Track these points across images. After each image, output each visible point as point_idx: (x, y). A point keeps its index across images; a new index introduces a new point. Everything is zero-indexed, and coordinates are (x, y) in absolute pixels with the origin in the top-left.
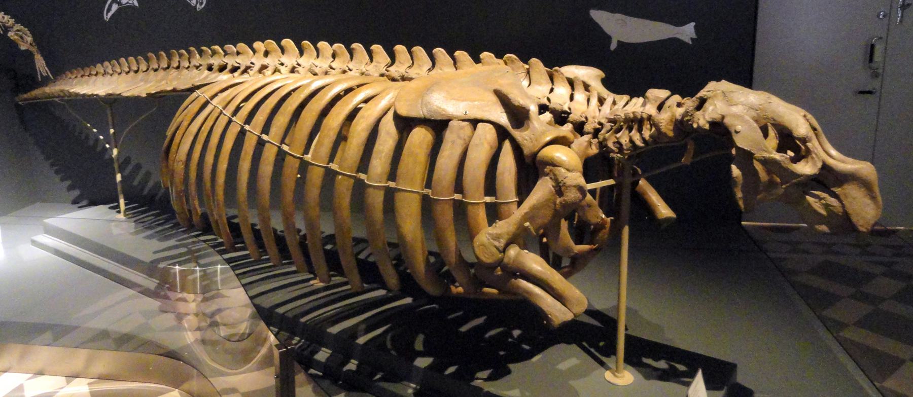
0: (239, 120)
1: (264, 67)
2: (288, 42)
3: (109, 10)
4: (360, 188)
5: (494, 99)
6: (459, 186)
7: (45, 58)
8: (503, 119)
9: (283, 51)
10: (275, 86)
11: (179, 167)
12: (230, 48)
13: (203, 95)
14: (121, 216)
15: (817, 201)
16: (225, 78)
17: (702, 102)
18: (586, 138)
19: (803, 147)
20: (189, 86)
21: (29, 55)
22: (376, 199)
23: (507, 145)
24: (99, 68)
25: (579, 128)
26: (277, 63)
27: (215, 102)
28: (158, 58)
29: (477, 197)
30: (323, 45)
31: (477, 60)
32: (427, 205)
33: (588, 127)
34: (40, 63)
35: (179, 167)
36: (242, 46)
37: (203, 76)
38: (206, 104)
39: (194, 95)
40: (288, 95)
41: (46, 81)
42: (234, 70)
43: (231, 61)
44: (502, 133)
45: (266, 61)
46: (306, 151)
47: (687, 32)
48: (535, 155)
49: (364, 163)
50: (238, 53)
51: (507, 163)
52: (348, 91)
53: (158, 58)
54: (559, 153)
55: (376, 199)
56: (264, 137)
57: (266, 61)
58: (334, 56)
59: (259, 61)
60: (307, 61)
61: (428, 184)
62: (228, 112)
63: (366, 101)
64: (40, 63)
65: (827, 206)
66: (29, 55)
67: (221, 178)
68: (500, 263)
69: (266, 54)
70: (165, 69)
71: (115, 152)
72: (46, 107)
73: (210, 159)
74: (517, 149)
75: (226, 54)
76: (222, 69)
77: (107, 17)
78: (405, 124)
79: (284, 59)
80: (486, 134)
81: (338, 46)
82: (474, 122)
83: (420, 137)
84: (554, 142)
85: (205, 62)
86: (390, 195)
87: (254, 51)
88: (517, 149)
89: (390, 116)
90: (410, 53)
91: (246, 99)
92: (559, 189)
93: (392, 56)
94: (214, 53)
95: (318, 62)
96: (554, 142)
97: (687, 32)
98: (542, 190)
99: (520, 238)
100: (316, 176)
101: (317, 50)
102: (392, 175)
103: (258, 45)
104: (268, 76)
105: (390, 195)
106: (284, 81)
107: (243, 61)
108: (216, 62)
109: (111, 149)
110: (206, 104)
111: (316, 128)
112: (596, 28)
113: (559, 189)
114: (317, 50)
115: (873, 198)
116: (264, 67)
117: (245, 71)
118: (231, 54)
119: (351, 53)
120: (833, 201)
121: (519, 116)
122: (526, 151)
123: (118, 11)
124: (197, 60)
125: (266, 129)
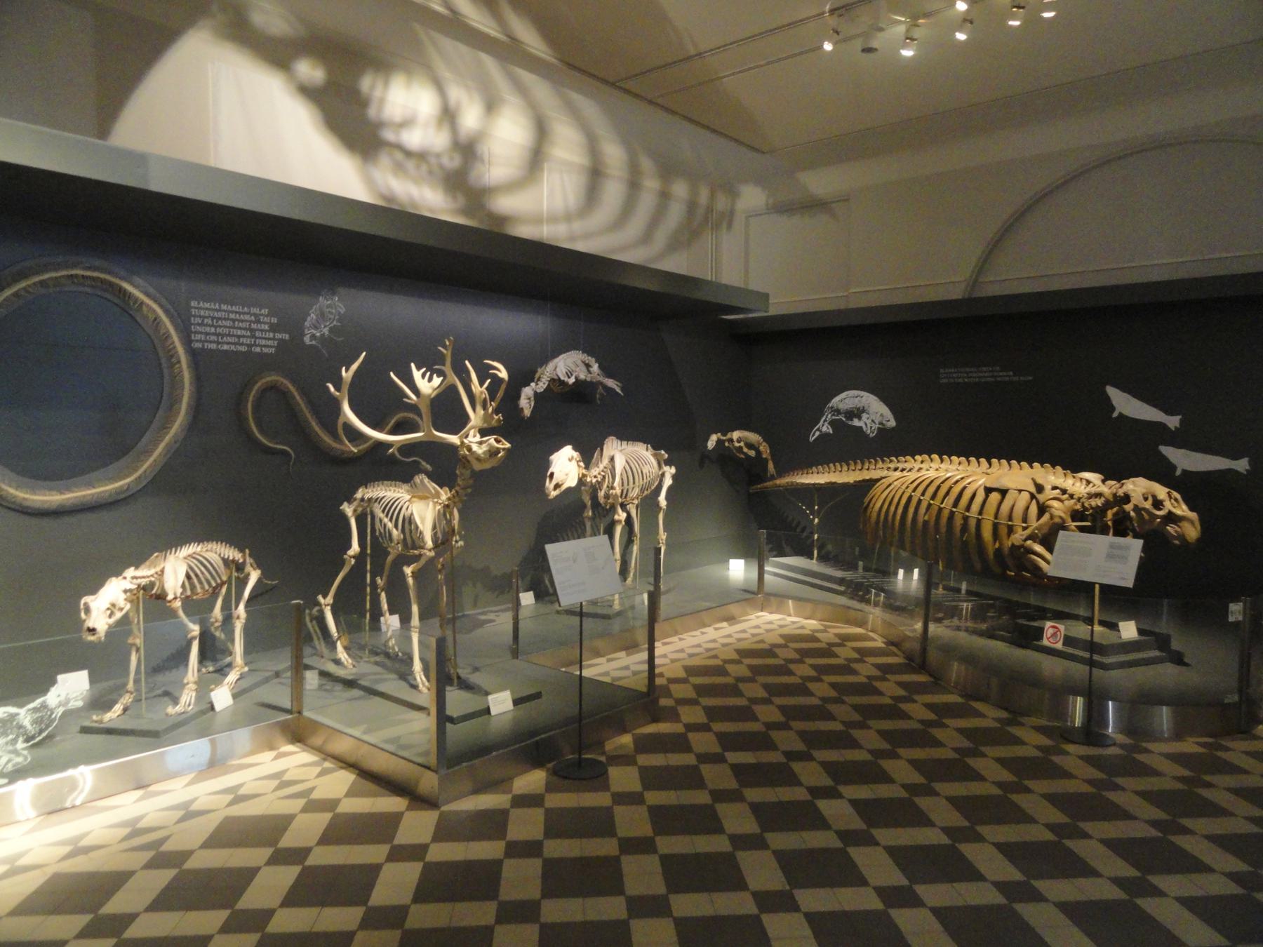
0: (910, 490)
1: (921, 469)
2: (935, 456)
3: (813, 435)
4: (966, 519)
5: (1031, 481)
6: (1010, 518)
7: (774, 463)
8: (1033, 490)
9: (932, 460)
10: (923, 478)
11: (874, 515)
12: (901, 458)
13: (885, 482)
14: (814, 561)
15: (1171, 529)
16: (898, 474)
17: (1123, 484)
18: (1074, 500)
19: (840, 417)
20: (879, 477)
21: (766, 460)
22: (973, 523)
23: (1034, 501)
24: (814, 469)
25: (1071, 496)
26: (928, 467)
27: (895, 483)
28: (855, 463)
29: (1017, 520)
30: (954, 458)
31: (1032, 467)
32: (996, 527)
33: (1075, 497)
34: (771, 466)
35: (874, 515)
36: (908, 458)
37: (885, 473)
38: (890, 485)
39: (882, 481)
40: (932, 481)
41: (772, 478)
42: (903, 470)
43: (901, 466)
44: (1033, 496)
45: (922, 466)
46: (942, 503)
47: (1242, 465)
48: (1044, 503)
49: (968, 508)
50: (906, 461)
51: (1034, 509)
52: (962, 478)
53: (855, 463)
54: (1055, 504)
55: (973, 523)
56: (922, 498)
57: (922, 466)
58: (960, 463)
59: (917, 466)
60: (943, 466)
61: (996, 517)
62: (904, 487)
63: (969, 484)
64: (771, 466)
65: (1176, 531)
66: (766, 460)
67: (898, 517)
68: (1022, 546)
69: (922, 462)
70: (860, 470)
71: (816, 520)
72: (764, 495)
73: (892, 508)
74: (1038, 502)
75: (898, 461)
76: (896, 469)
77: (812, 439)
78: (989, 490)
79: (932, 465)
80: (1026, 496)
81: (962, 459)
82: (1020, 491)
83: (995, 497)
84: (1054, 499)
85: (885, 466)
86: (979, 522)
87: (915, 461)
88: (1038, 502)
89: (983, 487)
90: (1000, 463)
91: (912, 483)
92: (1052, 517)
93: (990, 464)
94: (891, 461)
95: (950, 467)
96: (1054, 499)
97: (1242, 465)
98: (1046, 517)
99: (1031, 537)
100: (946, 514)
101: (951, 460)
102: (980, 513)
103: (917, 457)
104: (924, 472)
105: (979, 522)
106: (932, 474)
107: (908, 466)
108: (892, 466)
109: (814, 519)
110: (890, 485)
111: (947, 493)
112: (1165, 459)
113: (1052, 517)
114: (951, 460)
115: (1195, 528)
116: (920, 469)
117: (910, 470)
118: (902, 462)
119: (969, 462)
120: (1179, 530)
121: (1040, 488)
122: (1041, 502)
123: (819, 436)
124: (880, 464)
125: (923, 494)
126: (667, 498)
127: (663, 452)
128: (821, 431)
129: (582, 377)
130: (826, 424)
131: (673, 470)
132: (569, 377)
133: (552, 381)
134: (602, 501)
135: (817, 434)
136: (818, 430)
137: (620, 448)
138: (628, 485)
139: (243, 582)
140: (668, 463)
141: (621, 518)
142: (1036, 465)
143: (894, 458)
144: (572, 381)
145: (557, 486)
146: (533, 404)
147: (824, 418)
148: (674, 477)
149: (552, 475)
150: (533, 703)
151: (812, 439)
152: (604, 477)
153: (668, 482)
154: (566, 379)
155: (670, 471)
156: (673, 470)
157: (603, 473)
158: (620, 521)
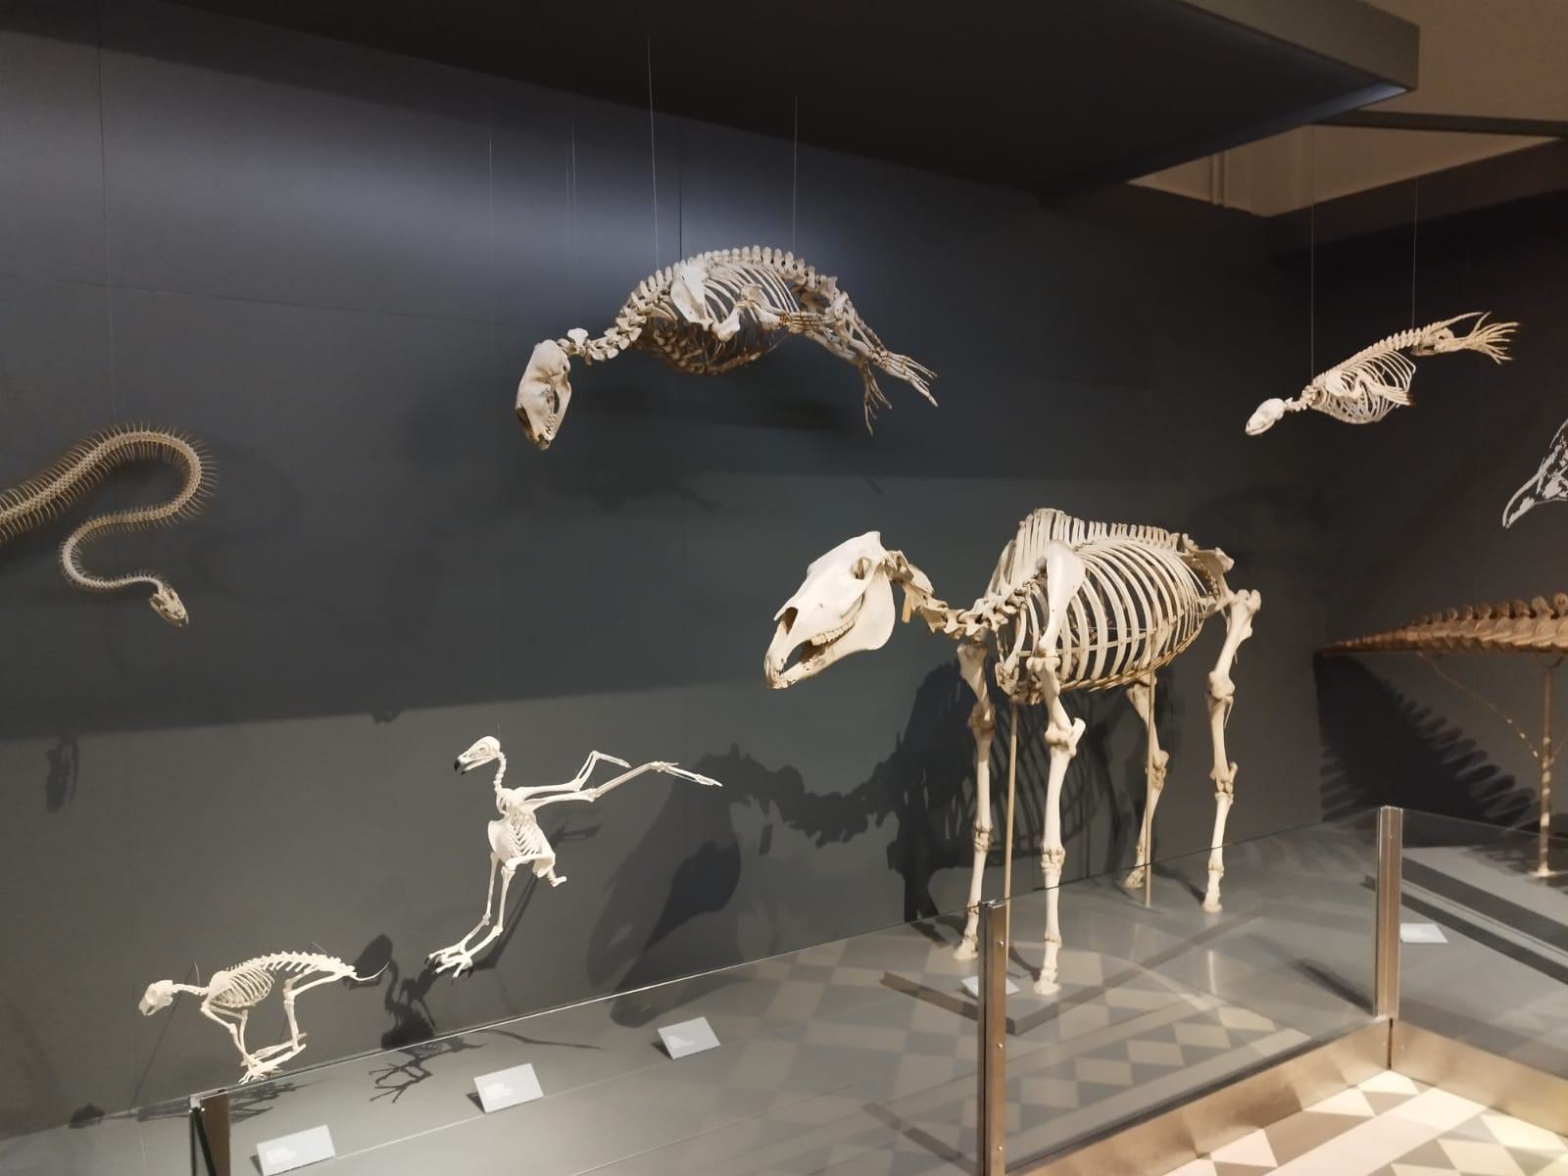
77: (1509, 520)
126: (1234, 674)
127: (1219, 552)
128: (1539, 497)
129: (768, 316)
130: (1558, 476)
131: (1254, 600)
132: (721, 317)
133: (651, 326)
134: (1008, 687)
135: (1527, 504)
136: (1531, 493)
137: (1078, 539)
138: (1129, 634)
139: (1037, 754)
140: (1236, 582)
141: (1064, 736)
142: (304, 953)
143: (1540, 603)
144: (728, 328)
145: (806, 651)
146: (565, 398)
147: (1551, 460)
148: (1257, 620)
149: (792, 614)
150: (1394, 1024)
151: (1509, 520)
152: (1013, 619)
153: (1240, 630)
154: (1347, 392)
155: (1243, 609)
156: (1254, 600)
157: (1010, 610)
158: (1063, 745)
